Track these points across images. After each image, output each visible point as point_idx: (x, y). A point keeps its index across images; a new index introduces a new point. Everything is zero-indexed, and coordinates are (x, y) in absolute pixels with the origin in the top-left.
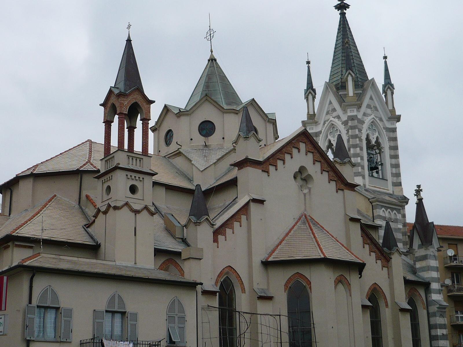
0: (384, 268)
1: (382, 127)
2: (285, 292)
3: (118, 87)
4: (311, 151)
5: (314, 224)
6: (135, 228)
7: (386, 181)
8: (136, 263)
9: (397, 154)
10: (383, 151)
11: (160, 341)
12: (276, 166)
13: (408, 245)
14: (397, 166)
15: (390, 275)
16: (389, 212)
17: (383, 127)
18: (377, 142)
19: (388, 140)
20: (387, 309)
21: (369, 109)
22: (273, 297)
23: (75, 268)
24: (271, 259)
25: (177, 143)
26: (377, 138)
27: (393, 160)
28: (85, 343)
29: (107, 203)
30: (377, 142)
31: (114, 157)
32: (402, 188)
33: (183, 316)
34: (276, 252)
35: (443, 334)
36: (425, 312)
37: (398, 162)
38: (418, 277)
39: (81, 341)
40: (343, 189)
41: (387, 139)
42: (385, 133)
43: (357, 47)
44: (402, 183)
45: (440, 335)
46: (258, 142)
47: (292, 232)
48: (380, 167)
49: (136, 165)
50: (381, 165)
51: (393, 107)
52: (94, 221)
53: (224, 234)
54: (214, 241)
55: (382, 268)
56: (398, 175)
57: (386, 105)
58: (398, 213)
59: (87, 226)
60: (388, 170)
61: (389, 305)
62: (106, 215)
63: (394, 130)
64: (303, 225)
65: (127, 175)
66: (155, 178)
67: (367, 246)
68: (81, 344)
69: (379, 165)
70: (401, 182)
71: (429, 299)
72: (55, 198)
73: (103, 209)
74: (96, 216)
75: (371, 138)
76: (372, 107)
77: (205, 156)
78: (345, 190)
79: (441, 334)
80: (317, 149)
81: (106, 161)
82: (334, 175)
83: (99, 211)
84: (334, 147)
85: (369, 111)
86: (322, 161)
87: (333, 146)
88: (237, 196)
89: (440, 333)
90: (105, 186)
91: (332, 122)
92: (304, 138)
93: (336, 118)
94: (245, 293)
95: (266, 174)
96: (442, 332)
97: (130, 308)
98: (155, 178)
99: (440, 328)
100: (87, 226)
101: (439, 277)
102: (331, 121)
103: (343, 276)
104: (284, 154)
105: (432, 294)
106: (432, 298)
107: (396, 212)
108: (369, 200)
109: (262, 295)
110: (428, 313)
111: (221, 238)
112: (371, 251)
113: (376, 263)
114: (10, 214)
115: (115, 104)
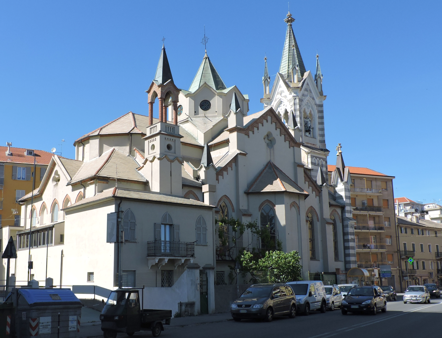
0: (317, 197)
1: (314, 103)
2: (259, 212)
3: (157, 80)
4: (274, 121)
5: (276, 169)
6: (171, 171)
7: (315, 139)
8: (171, 193)
9: (323, 122)
10: (314, 119)
11: (194, 242)
12: (253, 132)
13: (326, 179)
14: (323, 129)
15: (321, 201)
16: (318, 160)
17: (315, 104)
18: (310, 113)
19: (318, 113)
20: (318, 222)
21: (306, 92)
22: (252, 214)
23: (156, 199)
24: (250, 191)
25: (185, 114)
26: (310, 111)
27: (320, 125)
28: (151, 243)
29: (153, 155)
30: (310, 113)
31: (156, 126)
32: (325, 144)
33: (205, 227)
34: (254, 186)
35: (352, 239)
36: (341, 224)
37: (324, 127)
38: (337, 202)
39: (148, 242)
40: (294, 146)
41: (317, 112)
42: (316, 107)
43: (299, 49)
44: (325, 141)
45: (350, 239)
46: (243, 115)
47: (263, 173)
48: (311, 130)
49: (170, 131)
50: (312, 129)
51: (322, 90)
52: (143, 167)
53: (222, 175)
54: (217, 180)
55: (316, 197)
56: (323, 135)
57: (316, 87)
58: (323, 161)
59: (138, 169)
60: (317, 132)
61: (319, 220)
62: (152, 163)
63: (321, 106)
64: (269, 170)
65: (165, 138)
66: (182, 140)
67: (307, 183)
68: (148, 244)
69: (311, 129)
70: (325, 140)
71: (344, 217)
72: (115, 150)
73: (151, 159)
74: (145, 163)
75: (307, 110)
76: (308, 90)
77: (205, 123)
78: (295, 147)
79: (351, 239)
80: (278, 121)
81: (151, 129)
82: (288, 138)
83: (147, 160)
84: (282, 116)
85: (306, 93)
86: (281, 128)
87: (281, 115)
88: (228, 151)
89: (350, 238)
90: (151, 144)
91: (281, 100)
92: (271, 113)
93: (284, 97)
94: (234, 212)
95: (247, 136)
96: (351, 238)
97: (175, 222)
98: (182, 140)
99: (350, 235)
100: (138, 169)
101: (351, 203)
102: (281, 99)
103: (295, 203)
104: (258, 124)
105: (346, 213)
106: (346, 216)
107: (322, 160)
108: (305, 152)
109: (245, 213)
110: (343, 225)
111: (220, 177)
112: (309, 186)
113: (313, 193)
114: (83, 160)
115: (156, 91)
